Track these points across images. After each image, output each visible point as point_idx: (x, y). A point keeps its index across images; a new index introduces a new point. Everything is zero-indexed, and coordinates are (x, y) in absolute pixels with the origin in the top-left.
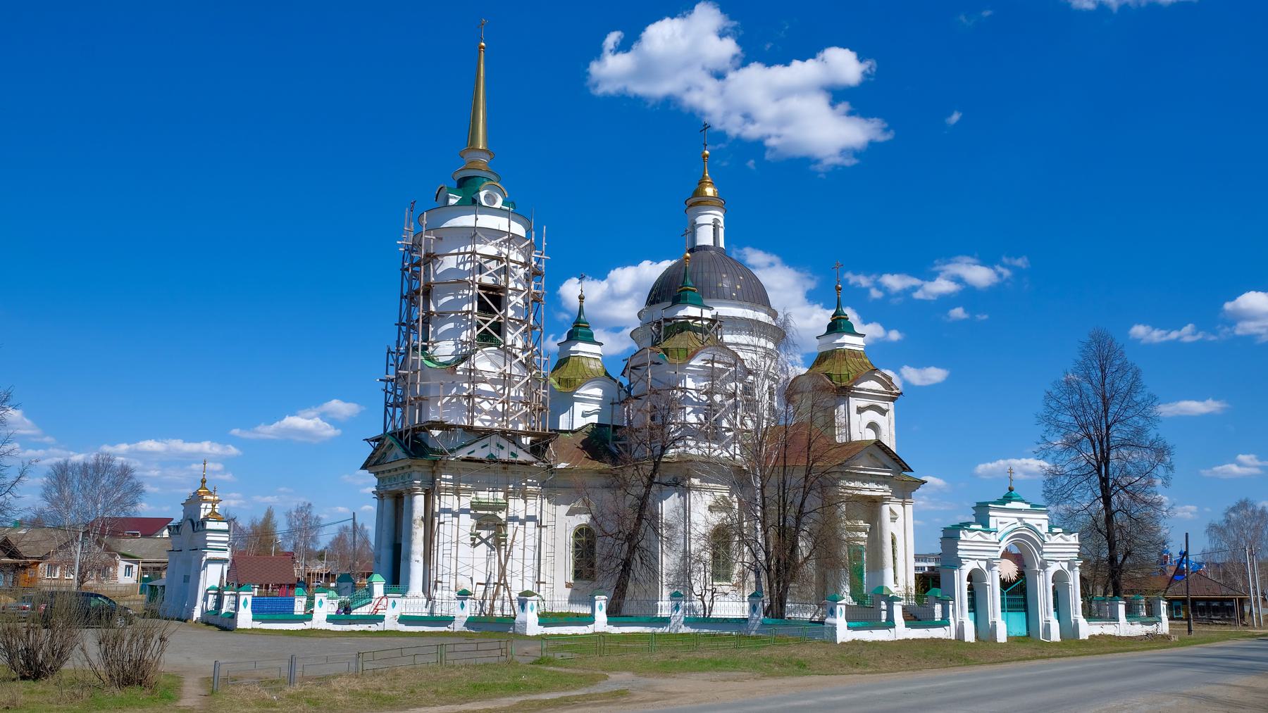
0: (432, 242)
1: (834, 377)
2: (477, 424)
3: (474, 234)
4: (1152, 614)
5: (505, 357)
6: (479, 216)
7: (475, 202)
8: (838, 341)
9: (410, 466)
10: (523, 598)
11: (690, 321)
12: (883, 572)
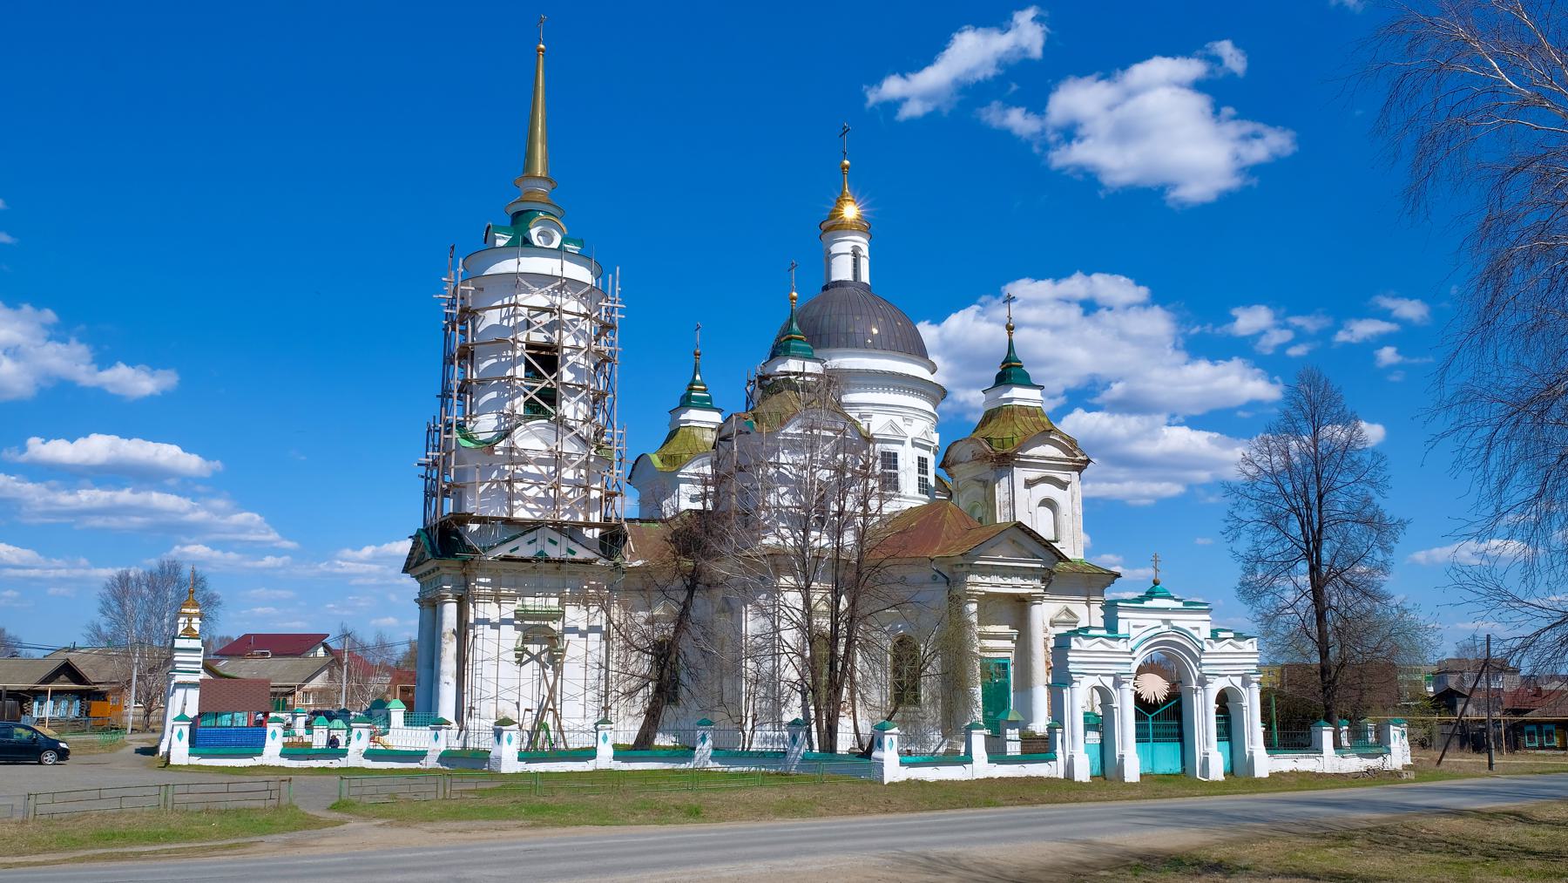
0: (470, 294)
1: (994, 442)
2: (521, 514)
3: (516, 282)
4: (1382, 745)
5: (557, 431)
6: (522, 259)
7: (527, 242)
8: (1005, 396)
9: (438, 569)
10: (498, 727)
11: (792, 377)
12: (1031, 691)
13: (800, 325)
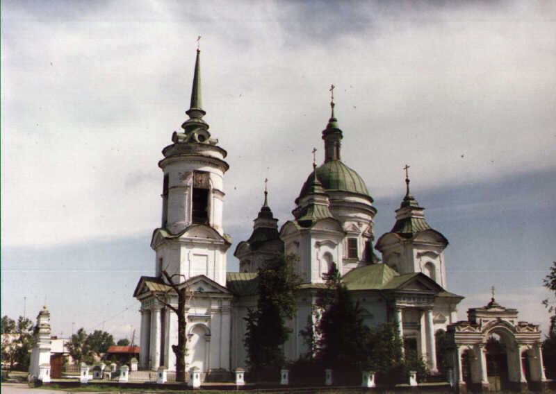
13: (319, 179)
